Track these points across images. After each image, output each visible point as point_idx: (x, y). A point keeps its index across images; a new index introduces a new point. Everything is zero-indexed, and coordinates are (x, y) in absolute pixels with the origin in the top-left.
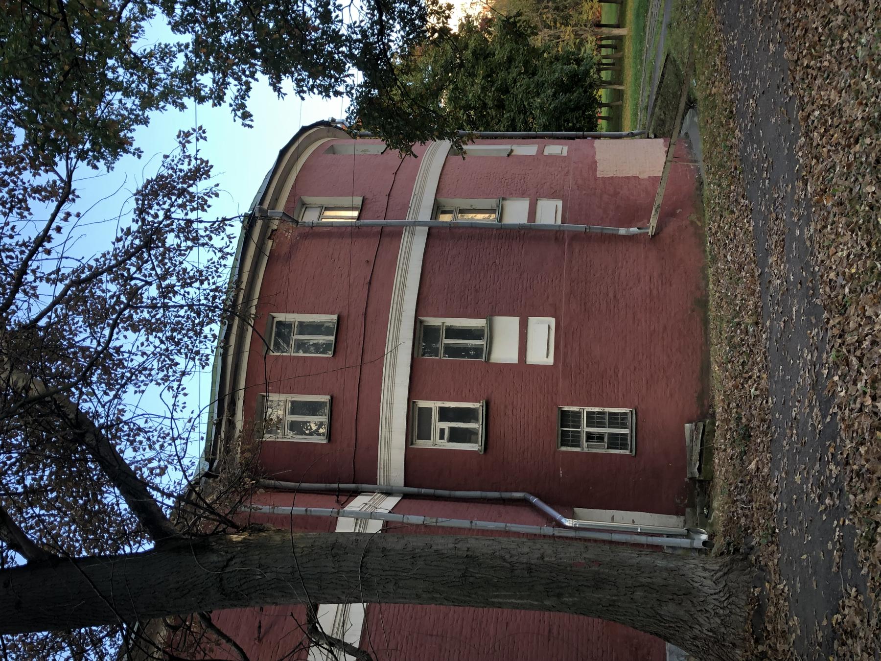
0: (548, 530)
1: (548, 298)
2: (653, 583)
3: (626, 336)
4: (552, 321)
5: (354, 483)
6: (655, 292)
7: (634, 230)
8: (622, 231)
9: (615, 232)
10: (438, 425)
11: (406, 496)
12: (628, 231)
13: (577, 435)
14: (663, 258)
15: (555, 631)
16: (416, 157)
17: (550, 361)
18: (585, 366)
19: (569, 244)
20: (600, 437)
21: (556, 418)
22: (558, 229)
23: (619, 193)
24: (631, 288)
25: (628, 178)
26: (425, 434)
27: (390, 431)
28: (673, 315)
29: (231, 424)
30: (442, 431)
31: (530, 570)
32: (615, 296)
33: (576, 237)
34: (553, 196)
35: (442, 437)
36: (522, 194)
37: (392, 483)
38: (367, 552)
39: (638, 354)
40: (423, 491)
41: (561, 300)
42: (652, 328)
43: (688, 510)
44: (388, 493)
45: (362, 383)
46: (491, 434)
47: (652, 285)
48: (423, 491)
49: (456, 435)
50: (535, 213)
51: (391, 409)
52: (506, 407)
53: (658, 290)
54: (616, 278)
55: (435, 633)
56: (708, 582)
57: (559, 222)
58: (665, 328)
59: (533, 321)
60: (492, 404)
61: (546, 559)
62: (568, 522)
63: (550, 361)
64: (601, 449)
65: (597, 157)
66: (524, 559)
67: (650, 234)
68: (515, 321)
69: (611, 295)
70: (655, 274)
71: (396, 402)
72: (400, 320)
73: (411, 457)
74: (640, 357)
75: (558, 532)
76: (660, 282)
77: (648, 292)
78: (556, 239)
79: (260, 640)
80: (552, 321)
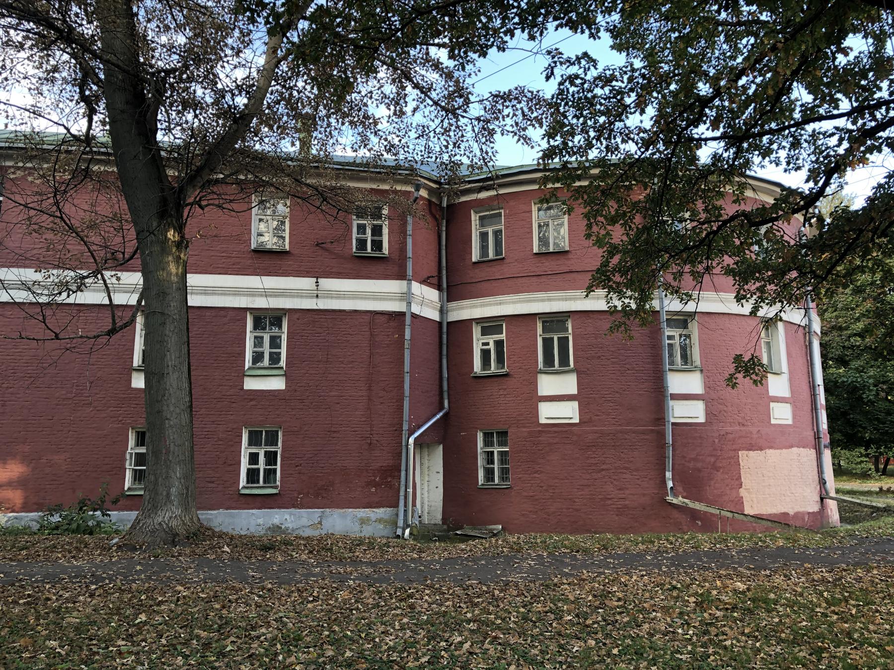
0: (405, 427)
1: (597, 416)
2: (158, 486)
3: (568, 479)
4: (576, 420)
5: (447, 286)
6: (609, 502)
7: (670, 484)
8: (669, 475)
9: (667, 468)
10: (491, 340)
11: (440, 324)
12: (669, 479)
13: (492, 445)
14: (644, 509)
15: (335, 435)
16: (587, 296)
17: (543, 421)
18: (540, 448)
19: (652, 430)
20: (492, 462)
21: (502, 428)
22: (666, 420)
23: (718, 471)
24: (612, 483)
25: (740, 477)
26: (485, 332)
27: (482, 306)
28: (590, 516)
29: (480, 190)
30: (487, 344)
31: (159, 412)
32: (603, 470)
33: (662, 435)
34: (708, 413)
35: (484, 344)
36: (707, 386)
37: (449, 313)
38: (162, 314)
39: (554, 489)
40: (445, 336)
41: (596, 426)
42: (577, 500)
43: (445, 527)
44: (442, 311)
45: (515, 280)
46: (486, 380)
47: (616, 500)
48: (445, 336)
49: (486, 354)
50: (686, 399)
51: (497, 304)
52: (505, 389)
53: (611, 505)
54: (622, 471)
55: (329, 357)
56: (160, 520)
57: (673, 420)
58: (577, 510)
59: (575, 404)
60: (506, 379)
61: (167, 421)
62: (411, 440)
63: (543, 421)
64: (481, 461)
65: (770, 452)
66: (165, 408)
67: (667, 498)
68: (574, 391)
69: (604, 467)
70: (627, 502)
71: (502, 306)
72: (566, 300)
73: (466, 324)
74: (551, 491)
75: (405, 433)
76: (620, 506)
77: (609, 497)
78: (659, 419)
79: (317, 245)
80: (576, 420)
